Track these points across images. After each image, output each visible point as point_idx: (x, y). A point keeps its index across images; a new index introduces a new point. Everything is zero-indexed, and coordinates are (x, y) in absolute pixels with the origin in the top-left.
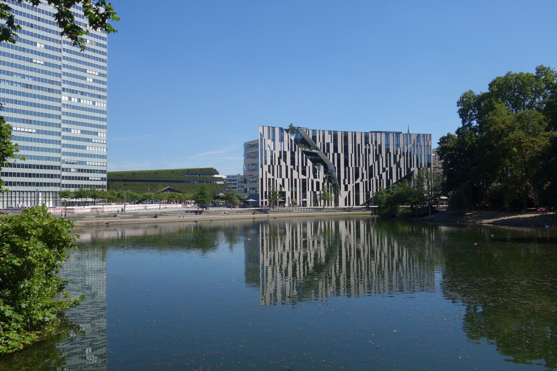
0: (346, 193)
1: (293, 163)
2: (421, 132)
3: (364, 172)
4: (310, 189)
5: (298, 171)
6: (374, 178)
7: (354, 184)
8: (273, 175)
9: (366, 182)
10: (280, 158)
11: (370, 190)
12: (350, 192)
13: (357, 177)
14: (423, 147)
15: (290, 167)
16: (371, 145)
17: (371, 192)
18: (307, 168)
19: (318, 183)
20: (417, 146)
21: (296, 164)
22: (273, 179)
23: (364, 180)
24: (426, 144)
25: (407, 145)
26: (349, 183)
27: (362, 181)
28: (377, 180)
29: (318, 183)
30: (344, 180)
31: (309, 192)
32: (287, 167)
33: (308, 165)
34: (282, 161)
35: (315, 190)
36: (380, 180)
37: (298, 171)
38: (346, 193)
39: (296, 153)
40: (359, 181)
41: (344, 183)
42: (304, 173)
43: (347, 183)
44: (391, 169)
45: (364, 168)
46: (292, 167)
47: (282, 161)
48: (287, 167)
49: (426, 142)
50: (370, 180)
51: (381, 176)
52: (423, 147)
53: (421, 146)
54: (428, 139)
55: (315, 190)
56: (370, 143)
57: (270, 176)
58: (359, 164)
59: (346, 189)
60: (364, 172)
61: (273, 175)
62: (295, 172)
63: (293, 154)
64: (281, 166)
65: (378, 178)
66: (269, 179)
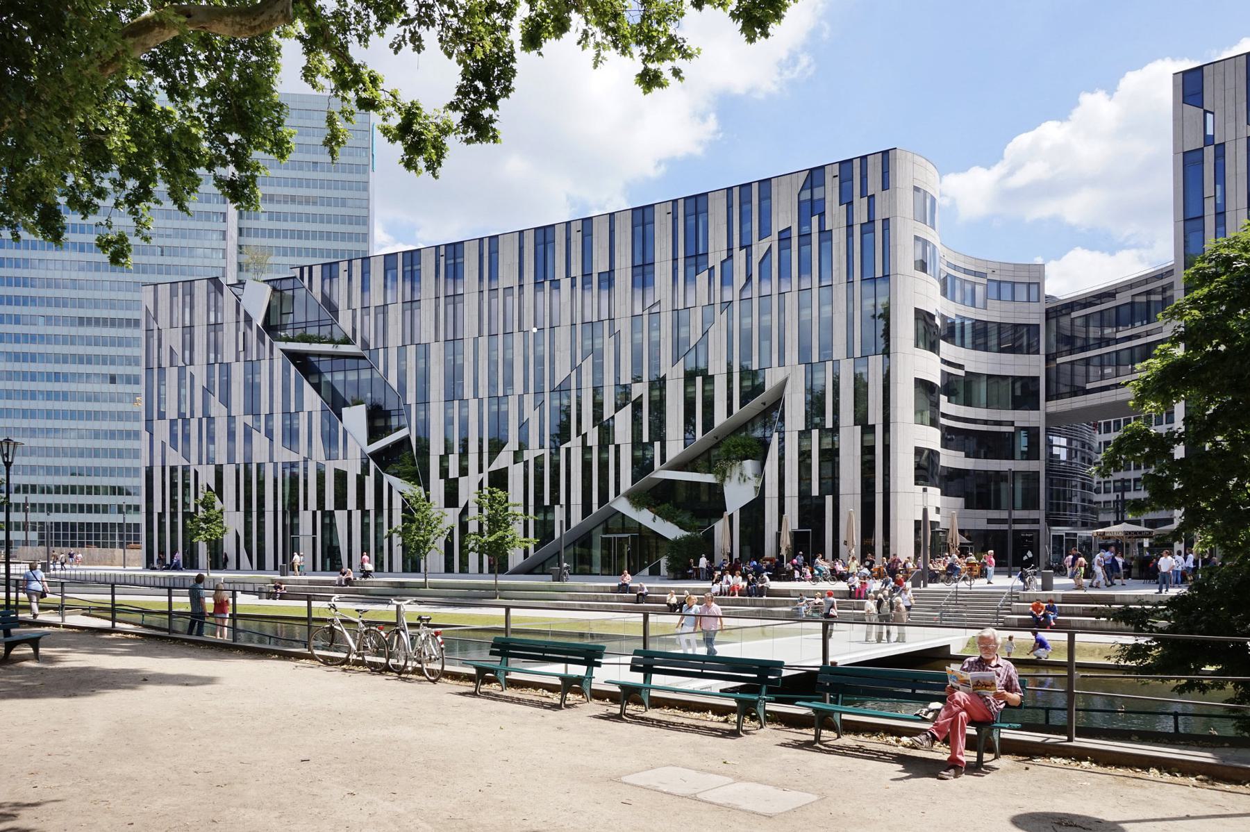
0: (451, 517)
1: (252, 408)
2: (828, 154)
3: (531, 414)
4: (313, 504)
5: (269, 434)
6: (575, 443)
7: (485, 476)
8: (186, 455)
9: (539, 463)
10: (207, 391)
11: (555, 500)
12: (465, 510)
13: (497, 446)
14: (839, 237)
15: (242, 420)
16: (473, 404)
17: (559, 514)
18: (303, 417)
19: (341, 477)
20: (805, 237)
21: (265, 409)
22: (186, 470)
23: (529, 455)
24: (860, 216)
25: (747, 247)
26: (464, 471)
27: (517, 456)
28: (586, 449)
29: (341, 477)
30: (444, 459)
31: (309, 514)
32: (231, 419)
33: (307, 407)
34: (215, 401)
35: (330, 505)
36: (603, 447)
37: (269, 434)
38: (451, 517)
39: (265, 365)
40: (504, 459)
41: (444, 472)
42: (291, 436)
43: (453, 472)
44: (659, 384)
45: (529, 400)
46: (249, 419)
47: (215, 401)
48: (231, 419)
49: (860, 205)
50: (555, 450)
51: (606, 431)
52: (839, 237)
53: (825, 234)
54: (874, 185)
55: (330, 505)
56: (468, 393)
57: (175, 458)
58: (509, 383)
59: (451, 499)
60: (531, 414)
61: (186, 455)
62: (259, 440)
63: (252, 368)
64: (211, 420)
65: (593, 440)
66: (173, 469)
